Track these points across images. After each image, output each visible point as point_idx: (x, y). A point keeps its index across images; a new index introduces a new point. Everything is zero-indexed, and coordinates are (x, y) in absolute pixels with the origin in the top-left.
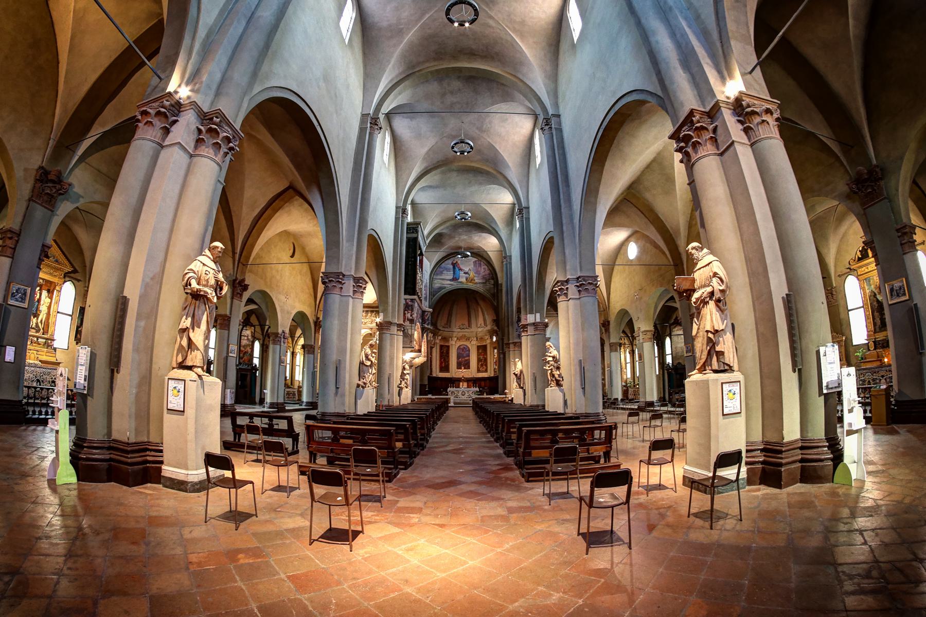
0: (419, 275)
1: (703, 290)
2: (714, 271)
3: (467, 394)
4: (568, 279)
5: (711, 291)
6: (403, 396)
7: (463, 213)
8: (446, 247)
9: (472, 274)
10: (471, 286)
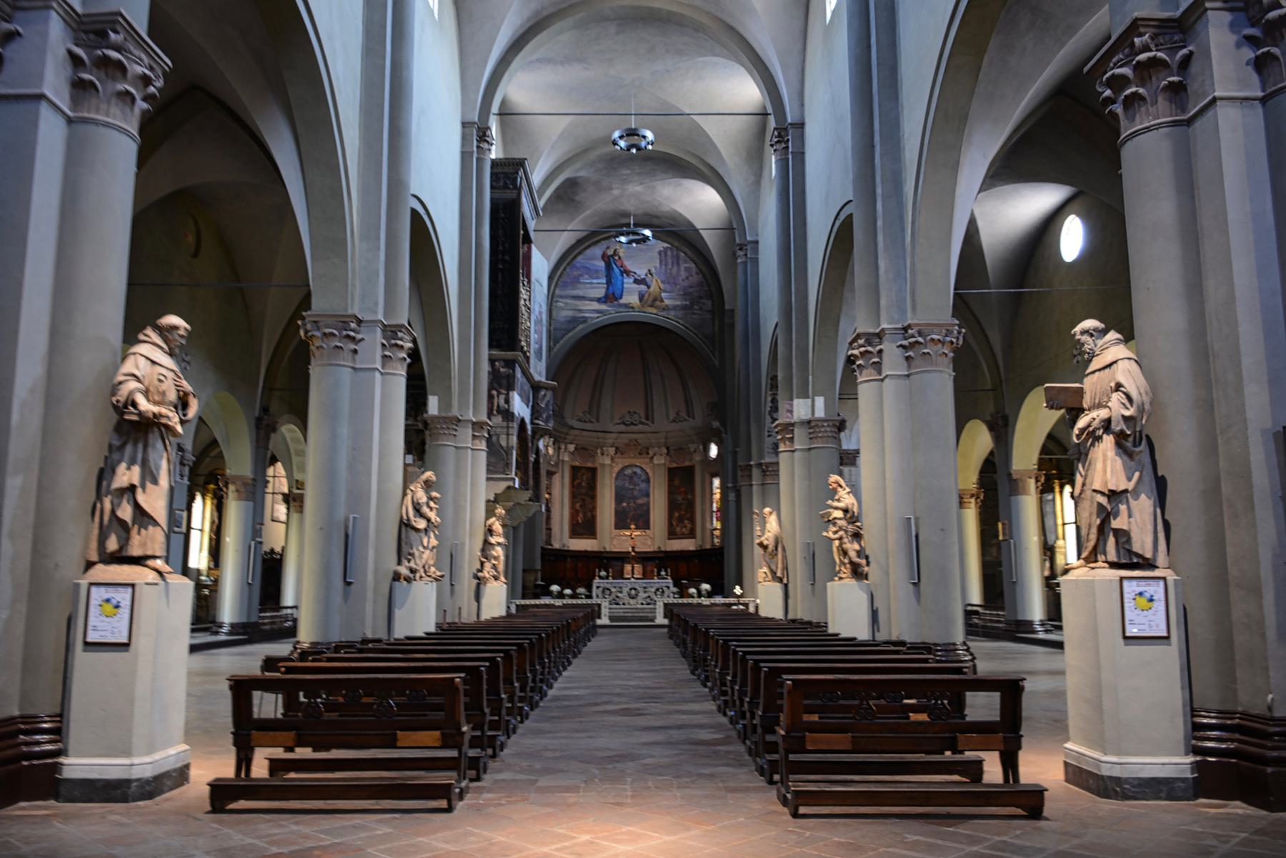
0: (524, 294)
1: (1094, 414)
2: (1117, 381)
3: (642, 595)
4: (883, 330)
5: (1107, 416)
6: (485, 601)
7: (631, 133)
8: (588, 212)
9: (655, 285)
10: (651, 314)
